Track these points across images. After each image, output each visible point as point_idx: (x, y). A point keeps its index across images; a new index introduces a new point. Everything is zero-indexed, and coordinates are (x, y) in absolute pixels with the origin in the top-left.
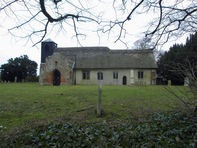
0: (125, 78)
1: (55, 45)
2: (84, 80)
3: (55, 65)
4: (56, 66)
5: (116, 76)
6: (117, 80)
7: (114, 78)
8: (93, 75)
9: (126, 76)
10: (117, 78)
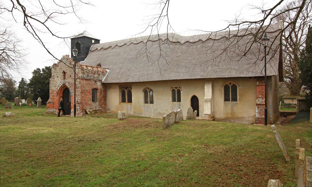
0: (195, 103)
1: (93, 41)
2: (174, 103)
3: (63, 77)
4: (64, 79)
5: (176, 97)
6: (180, 105)
7: (174, 100)
8: (138, 96)
9: (196, 95)
10: (179, 100)
